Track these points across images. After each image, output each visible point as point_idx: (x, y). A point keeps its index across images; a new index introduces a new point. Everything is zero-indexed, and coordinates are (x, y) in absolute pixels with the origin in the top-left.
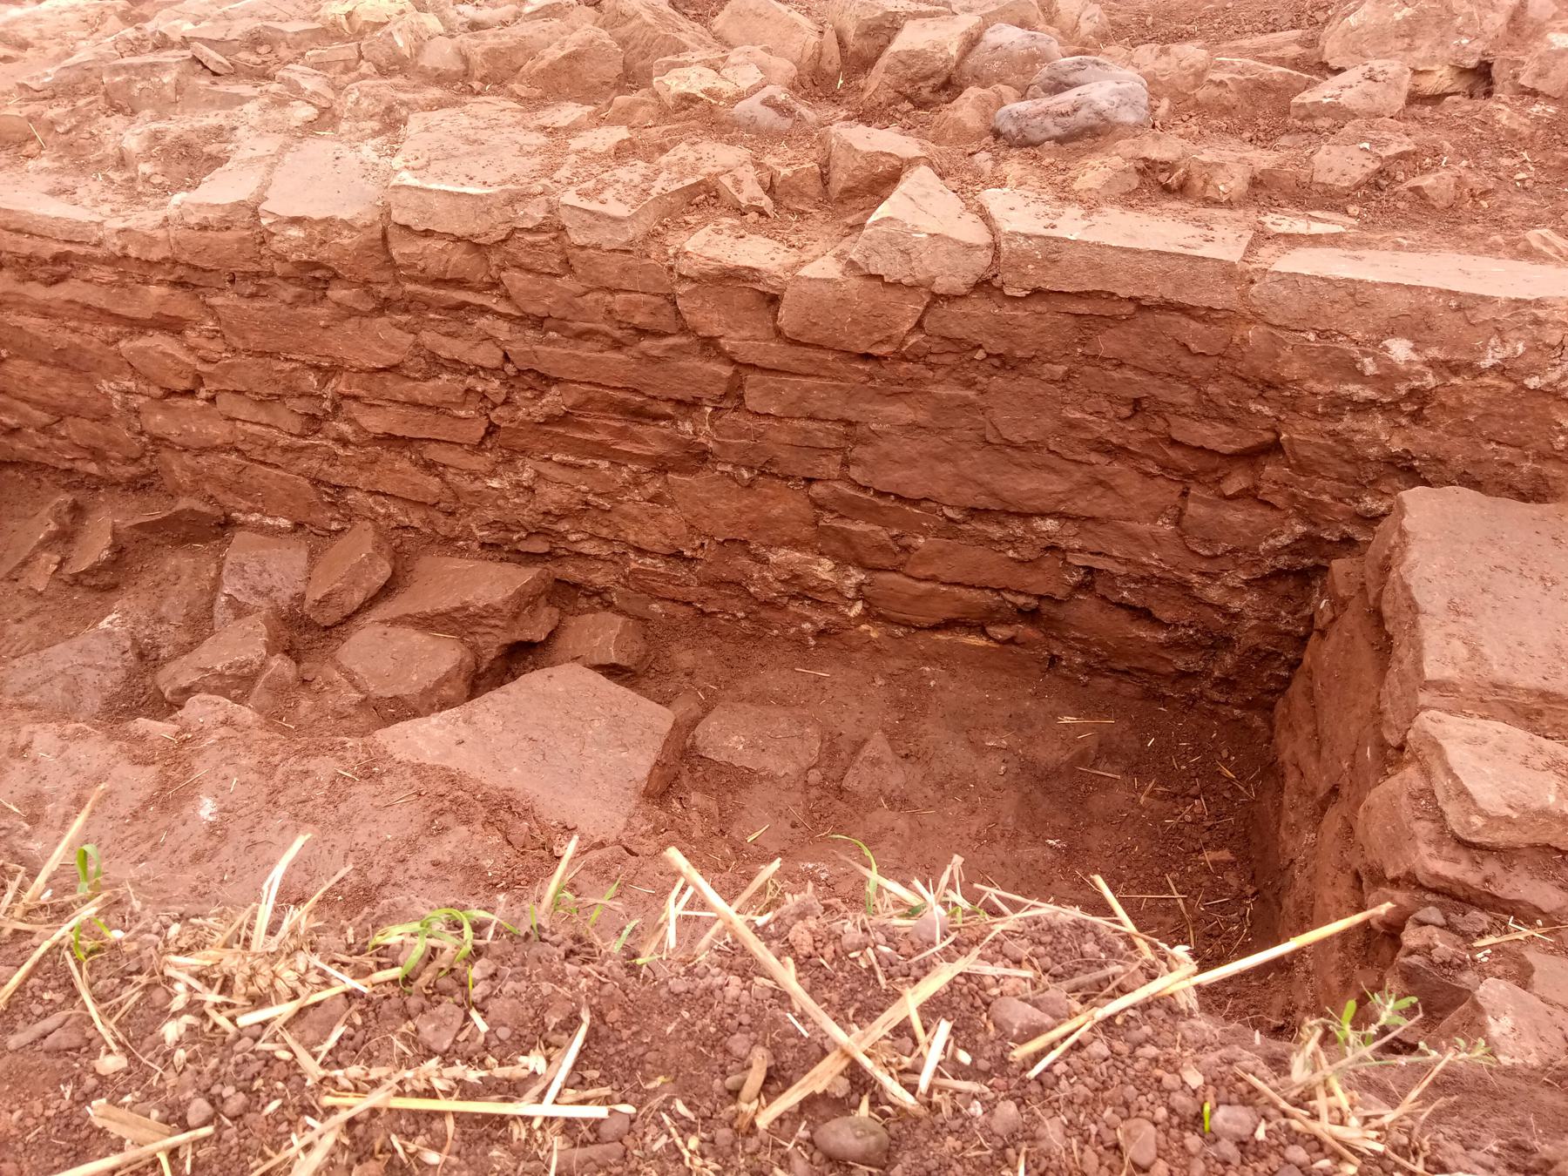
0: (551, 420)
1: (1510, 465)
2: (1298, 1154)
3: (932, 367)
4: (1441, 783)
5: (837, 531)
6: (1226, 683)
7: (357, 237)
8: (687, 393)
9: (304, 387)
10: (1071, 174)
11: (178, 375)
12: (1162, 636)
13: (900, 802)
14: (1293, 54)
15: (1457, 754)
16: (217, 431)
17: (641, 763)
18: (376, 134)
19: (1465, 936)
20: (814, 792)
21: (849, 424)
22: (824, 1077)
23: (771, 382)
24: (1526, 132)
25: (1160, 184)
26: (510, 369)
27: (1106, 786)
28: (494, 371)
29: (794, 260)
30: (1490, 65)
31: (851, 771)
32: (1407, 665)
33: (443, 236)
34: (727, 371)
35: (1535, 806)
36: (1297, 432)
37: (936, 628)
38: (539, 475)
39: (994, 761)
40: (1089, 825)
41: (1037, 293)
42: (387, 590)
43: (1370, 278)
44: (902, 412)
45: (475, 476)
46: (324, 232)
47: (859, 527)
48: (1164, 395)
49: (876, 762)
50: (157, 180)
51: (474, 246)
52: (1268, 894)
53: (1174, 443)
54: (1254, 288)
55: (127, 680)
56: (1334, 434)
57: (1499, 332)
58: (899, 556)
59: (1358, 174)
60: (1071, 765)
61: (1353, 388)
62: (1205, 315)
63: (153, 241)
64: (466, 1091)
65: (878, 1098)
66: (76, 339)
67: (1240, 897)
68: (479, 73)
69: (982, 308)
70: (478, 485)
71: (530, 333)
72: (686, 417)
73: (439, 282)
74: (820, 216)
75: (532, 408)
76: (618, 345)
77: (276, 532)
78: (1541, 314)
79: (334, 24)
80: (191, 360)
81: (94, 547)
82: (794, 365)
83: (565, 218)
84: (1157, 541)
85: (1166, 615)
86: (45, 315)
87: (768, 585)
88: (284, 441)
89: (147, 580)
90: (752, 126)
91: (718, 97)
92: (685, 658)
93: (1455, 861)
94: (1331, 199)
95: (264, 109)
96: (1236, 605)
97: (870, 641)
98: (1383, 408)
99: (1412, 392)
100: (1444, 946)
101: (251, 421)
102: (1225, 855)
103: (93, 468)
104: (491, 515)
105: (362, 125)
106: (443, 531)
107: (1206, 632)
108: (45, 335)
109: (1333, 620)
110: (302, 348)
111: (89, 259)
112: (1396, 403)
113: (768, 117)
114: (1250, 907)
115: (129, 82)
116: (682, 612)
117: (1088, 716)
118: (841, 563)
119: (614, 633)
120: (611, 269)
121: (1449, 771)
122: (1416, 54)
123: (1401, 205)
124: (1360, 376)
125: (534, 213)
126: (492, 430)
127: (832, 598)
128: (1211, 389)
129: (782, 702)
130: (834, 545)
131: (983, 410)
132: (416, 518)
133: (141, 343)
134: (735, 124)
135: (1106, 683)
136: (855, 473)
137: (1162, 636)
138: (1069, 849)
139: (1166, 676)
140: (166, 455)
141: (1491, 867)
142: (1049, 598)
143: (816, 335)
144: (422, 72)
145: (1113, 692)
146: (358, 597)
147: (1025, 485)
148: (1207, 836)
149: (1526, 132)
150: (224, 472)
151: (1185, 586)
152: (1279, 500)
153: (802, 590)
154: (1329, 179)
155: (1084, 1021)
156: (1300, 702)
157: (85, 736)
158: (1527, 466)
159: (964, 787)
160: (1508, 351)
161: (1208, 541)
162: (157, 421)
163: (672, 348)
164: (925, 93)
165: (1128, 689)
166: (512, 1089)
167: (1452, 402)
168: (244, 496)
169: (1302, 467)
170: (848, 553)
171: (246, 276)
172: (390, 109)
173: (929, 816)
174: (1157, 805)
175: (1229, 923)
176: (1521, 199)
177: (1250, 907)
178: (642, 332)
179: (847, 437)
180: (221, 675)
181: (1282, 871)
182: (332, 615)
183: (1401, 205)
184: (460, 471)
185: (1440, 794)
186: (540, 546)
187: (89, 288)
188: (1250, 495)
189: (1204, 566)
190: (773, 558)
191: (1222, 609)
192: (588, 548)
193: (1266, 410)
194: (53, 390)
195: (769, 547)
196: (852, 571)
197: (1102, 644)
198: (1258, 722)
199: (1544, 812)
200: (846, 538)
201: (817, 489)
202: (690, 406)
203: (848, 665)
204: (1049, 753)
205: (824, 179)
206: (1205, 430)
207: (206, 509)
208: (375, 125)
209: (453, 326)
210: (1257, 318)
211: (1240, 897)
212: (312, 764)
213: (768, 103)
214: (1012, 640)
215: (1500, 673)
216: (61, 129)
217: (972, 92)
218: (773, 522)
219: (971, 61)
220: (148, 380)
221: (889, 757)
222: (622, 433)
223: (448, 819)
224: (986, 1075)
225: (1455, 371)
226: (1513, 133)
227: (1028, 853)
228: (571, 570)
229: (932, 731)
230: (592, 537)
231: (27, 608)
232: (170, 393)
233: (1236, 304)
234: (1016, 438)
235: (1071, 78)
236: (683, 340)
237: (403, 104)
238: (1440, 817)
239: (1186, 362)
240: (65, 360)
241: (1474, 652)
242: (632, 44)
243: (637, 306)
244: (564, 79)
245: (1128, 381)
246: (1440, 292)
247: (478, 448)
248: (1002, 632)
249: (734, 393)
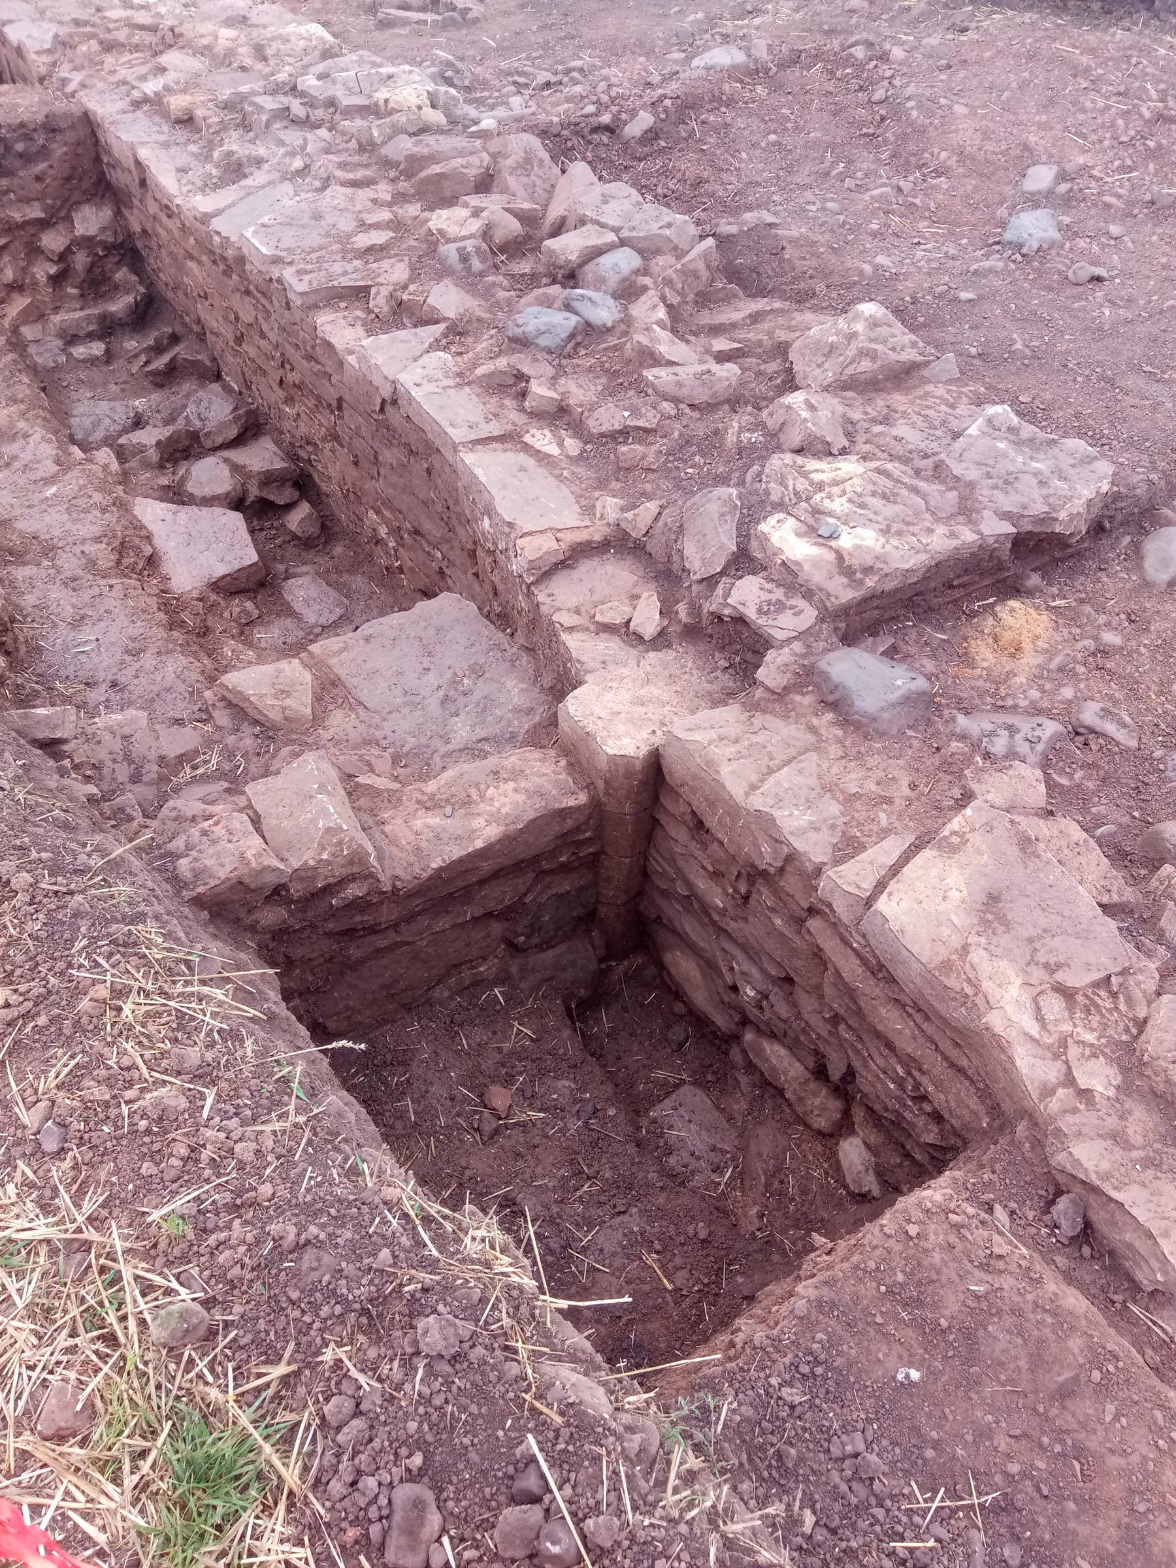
146: (219, 440)
244: (431, 188)
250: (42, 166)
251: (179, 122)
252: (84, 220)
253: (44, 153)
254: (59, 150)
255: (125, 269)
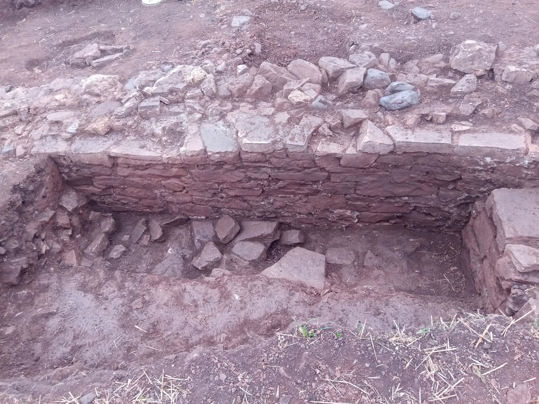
0: (280, 188)
1: (513, 180)
2: (535, 340)
3: (378, 169)
4: (514, 261)
5: (352, 205)
6: (449, 227)
7: (233, 155)
8: (316, 179)
9: (214, 187)
10: (405, 119)
11: (179, 188)
12: (433, 219)
13: (379, 267)
14: (443, 66)
15: (516, 254)
16: (188, 199)
17: (322, 269)
18: (219, 120)
19: (522, 289)
20: (357, 267)
21: (357, 182)
22: (480, 341)
23: (337, 175)
24: (506, 93)
25: (425, 120)
26: (270, 179)
27: (424, 255)
28: (266, 180)
29: (343, 149)
30: (493, 69)
31: (365, 261)
32: (501, 234)
33: (255, 153)
34: (327, 174)
35: (533, 264)
36: (465, 176)
37: (377, 222)
38: (275, 200)
39: (397, 253)
40: (423, 265)
41: (404, 153)
42: (239, 233)
43: (481, 146)
44: (370, 178)
45: (257, 202)
46: (225, 154)
47: (359, 203)
48: (434, 170)
49: (371, 258)
50: (169, 141)
51: (263, 154)
52: (470, 277)
53: (436, 179)
54: (455, 149)
55: (184, 266)
56: (474, 176)
57: (510, 156)
58: (368, 208)
59: (470, 111)
60: (415, 251)
61: (478, 167)
62: (444, 155)
63: (177, 159)
64: (439, 349)
65: (487, 342)
66: (149, 182)
67: (461, 277)
68: (236, 95)
69: (392, 157)
70: (258, 204)
71: (276, 170)
72: (315, 184)
73: (255, 162)
74: (343, 133)
75: (274, 186)
76: (299, 171)
77: (201, 220)
78: (518, 152)
79: (190, 83)
80: (182, 184)
81: (158, 233)
82: (344, 171)
83: (288, 147)
84: (432, 199)
85: (435, 214)
86: (140, 177)
87: (334, 218)
88: (206, 199)
89: (172, 238)
90: (317, 108)
91: (307, 101)
92: (313, 237)
93: (519, 276)
94: (465, 118)
95: (187, 116)
96: (451, 211)
97: (360, 227)
98: (485, 171)
99: (491, 168)
100: (520, 293)
101: (197, 196)
102: (456, 268)
103: (148, 210)
104: (261, 210)
105: (215, 117)
106: (247, 215)
107: (445, 217)
108: (140, 182)
109: (477, 216)
110: (215, 179)
111: (157, 164)
112: (488, 170)
113: (321, 105)
114: (464, 279)
115: (146, 111)
116: (310, 226)
117: (416, 238)
118: (353, 211)
119: (297, 235)
120: (299, 156)
121: (515, 258)
122: (474, 66)
123: (481, 118)
124: (480, 165)
125: (280, 146)
126: (263, 191)
127: (350, 219)
128: (445, 169)
129: (342, 246)
130: (351, 208)
131: (390, 176)
132: (240, 212)
133: (168, 181)
134: (313, 108)
135: (419, 230)
136: (358, 192)
137: (433, 219)
138: (421, 272)
139: (434, 227)
140: (171, 205)
141: (526, 276)
142: (405, 213)
143: (350, 165)
144: (221, 97)
145: (421, 231)
146: (233, 236)
147: (400, 191)
148: (450, 264)
149: (506, 93)
150: (188, 208)
151: (439, 209)
152: (461, 189)
153: (342, 218)
154: (464, 113)
155: (506, 330)
156: (470, 233)
157: (197, 284)
158: (517, 180)
159: (392, 261)
160: (512, 159)
161: (445, 199)
162: (170, 198)
163: (313, 171)
164: (356, 90)
165: (425, 230)
166: (444, 348)
167: (500, 169)
168: (193, 213)
169: (467, 183)
170: (354, 208)
171: (201, 165)
172: (221, 112)
173: (387, 270)
174: (437, 257)
175: (460, 284)
176: (507, 113)
177: (464, 279)
178: (305, 168)
179: (356, 185)
180: (213, 262)
181: (473, 273)
182: (227, 241)
183: (481, 118)
184: (253, 201)
185: (514, 263)
186: (274, 215)
187: (156, 170)
188: (454, 189)
189: (444, 204)
190: (335, 212)
191: (448, 212)
192: (286, 214)
193: (458, 172)
194: (140, 194)
195: (334, 209)
196: (356, 212)
197: (418, 222)
198: (457, 235)
199: (534, 265)
200: (355, 206)
201: (347, 196)
202: (315, 182)
203: (355, 233)
204: (410, 249)
205: (342, 124)
206: (444, 177)
207: (184, 217)
208: (218, 117)
209: (256, 171)
210: (456, 155)
211: (461, 277)
212: (255, 283)
213: (320, 101)
214: (395, 223)
215: (520, 234)
216: (133, 127)
217: (370, 93)
218: (335, 204)
219: (366, 81)
220: (169, 189)
221: (373, 256)
222: (298, 189)
223: (293, 291)
224: (498, 337)
225: (501, 163)
226: (503, 94)
227: (412, 275)
228: (281, 220)
229: (380, 248)
230: (287, 212)
231: (145, 250)
232: (175, 192)
233: (451, 152)
234: (398, 181)
235: (397, 89)
236: (316, 169)
237: (224, 111)
238: (515, 267)
239: (440, 164)
240: (145, 187)
241: (515, 230)
242: (270, 79)
243: (305, 163)
244: (259, 95)
245: (426, 168)
246: (496, 148)
247: (259, 196)
248: (393, 221)
249: (328, 178)
250: (43, 190)
251: (108, 133)
252: (67, 203)
253: (41, 185)
254: (47, 179)
255: (92, 212)
